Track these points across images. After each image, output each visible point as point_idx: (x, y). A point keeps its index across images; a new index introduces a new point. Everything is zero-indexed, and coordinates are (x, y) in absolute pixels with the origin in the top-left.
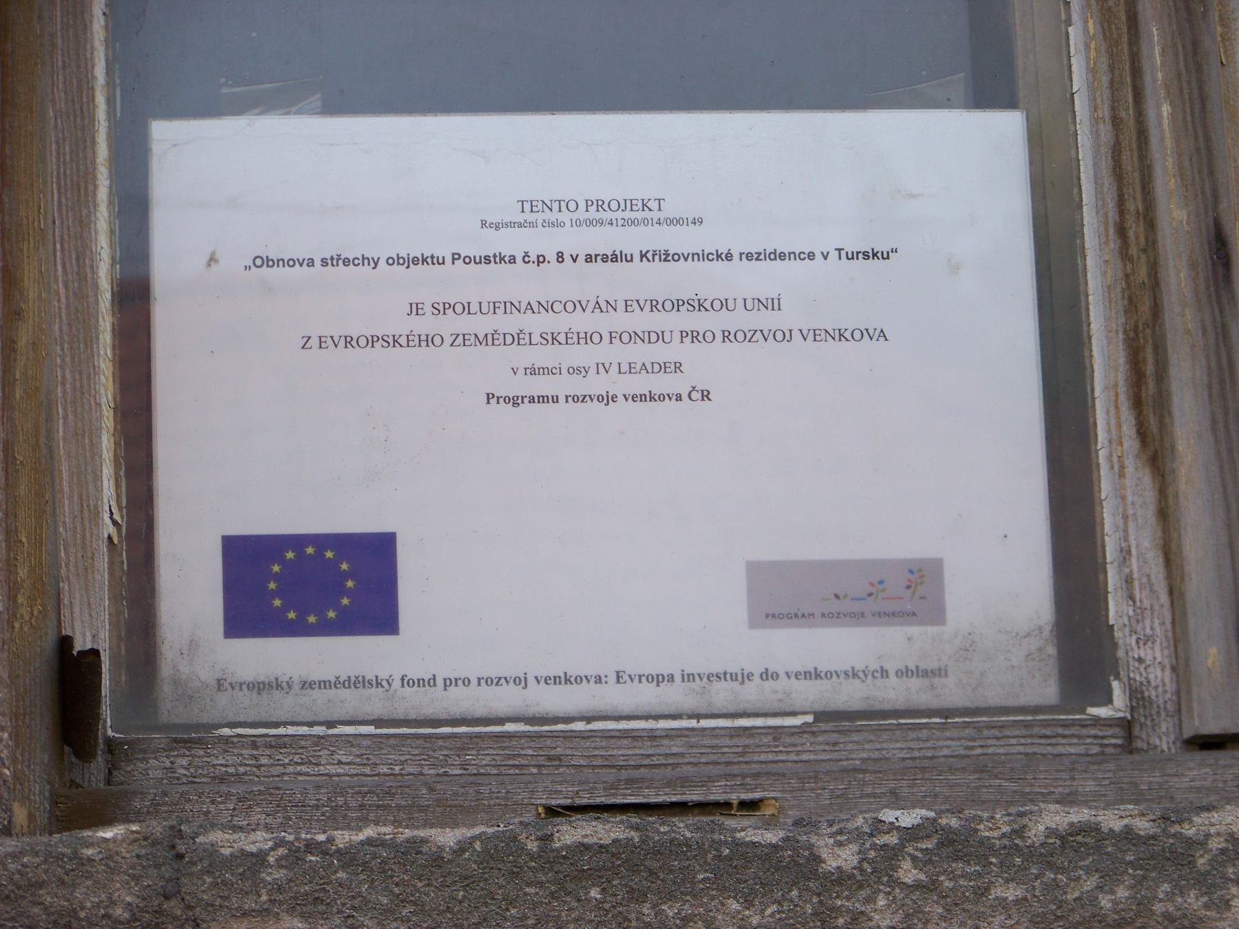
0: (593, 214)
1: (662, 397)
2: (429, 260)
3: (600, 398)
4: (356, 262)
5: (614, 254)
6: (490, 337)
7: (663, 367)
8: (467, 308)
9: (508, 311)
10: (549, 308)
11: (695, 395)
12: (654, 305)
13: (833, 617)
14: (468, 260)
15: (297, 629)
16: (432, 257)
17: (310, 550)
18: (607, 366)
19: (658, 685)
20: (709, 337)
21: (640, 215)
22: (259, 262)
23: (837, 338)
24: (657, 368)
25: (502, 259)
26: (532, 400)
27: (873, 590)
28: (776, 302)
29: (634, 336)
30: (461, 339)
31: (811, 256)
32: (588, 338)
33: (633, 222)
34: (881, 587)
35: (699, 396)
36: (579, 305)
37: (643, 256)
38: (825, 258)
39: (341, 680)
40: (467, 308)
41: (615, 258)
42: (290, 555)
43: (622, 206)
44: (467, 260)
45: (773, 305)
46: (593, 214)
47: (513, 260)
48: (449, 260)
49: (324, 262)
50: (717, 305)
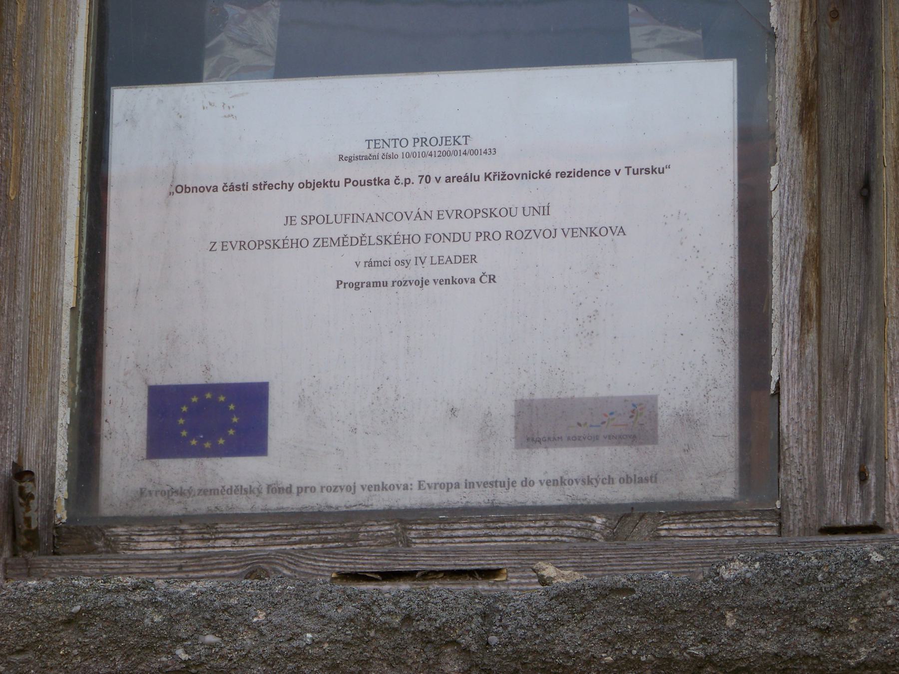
0: (418, 148)
1: (461, 281)
2: (329, 184)
3: (417, 283)
4: (277, 186)
5: (466, 176)
6: (341, 240)
7: (463, 259)
8: (326, 219)
9: (542, 209)
10: (384, 218)
11: (485, 279)
12: (459, 214)
13: (576, 440)
14: (356, 183)
15: (200, 453)
16: (331, 182)
17: (208, 396)
18: (423, 259)
19: (448, 491)
20: (497, 236)
21: (452, 148)
22: (179, 189)
23: (589, 234)
24: (458, 259)
25: (380, 182)
26: (369, 285)
27: (605, 419)
28: (546, 208)
29: (444, 237)
30: (321, 242)
31: (607, 173)
32: (410, 239)
33: (446, 153)
34: (611, 417)
35: (487, 279)
36: (406, 215)
37: (487, 176)
38: (618, 174)
39: (226, 488)
40: (326, 219)
41: (467, 179)
42: (195, 399)
43: (440, 142)
44: (355, 183)
45: (545, 210)
46: (418, 148)
47: (388, 182)
48: (342, 183)
49: (255, 187)
50: (503, 212)
